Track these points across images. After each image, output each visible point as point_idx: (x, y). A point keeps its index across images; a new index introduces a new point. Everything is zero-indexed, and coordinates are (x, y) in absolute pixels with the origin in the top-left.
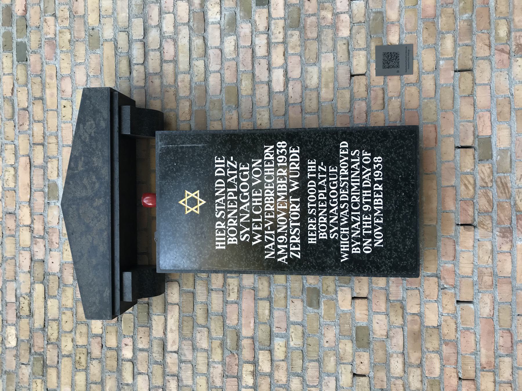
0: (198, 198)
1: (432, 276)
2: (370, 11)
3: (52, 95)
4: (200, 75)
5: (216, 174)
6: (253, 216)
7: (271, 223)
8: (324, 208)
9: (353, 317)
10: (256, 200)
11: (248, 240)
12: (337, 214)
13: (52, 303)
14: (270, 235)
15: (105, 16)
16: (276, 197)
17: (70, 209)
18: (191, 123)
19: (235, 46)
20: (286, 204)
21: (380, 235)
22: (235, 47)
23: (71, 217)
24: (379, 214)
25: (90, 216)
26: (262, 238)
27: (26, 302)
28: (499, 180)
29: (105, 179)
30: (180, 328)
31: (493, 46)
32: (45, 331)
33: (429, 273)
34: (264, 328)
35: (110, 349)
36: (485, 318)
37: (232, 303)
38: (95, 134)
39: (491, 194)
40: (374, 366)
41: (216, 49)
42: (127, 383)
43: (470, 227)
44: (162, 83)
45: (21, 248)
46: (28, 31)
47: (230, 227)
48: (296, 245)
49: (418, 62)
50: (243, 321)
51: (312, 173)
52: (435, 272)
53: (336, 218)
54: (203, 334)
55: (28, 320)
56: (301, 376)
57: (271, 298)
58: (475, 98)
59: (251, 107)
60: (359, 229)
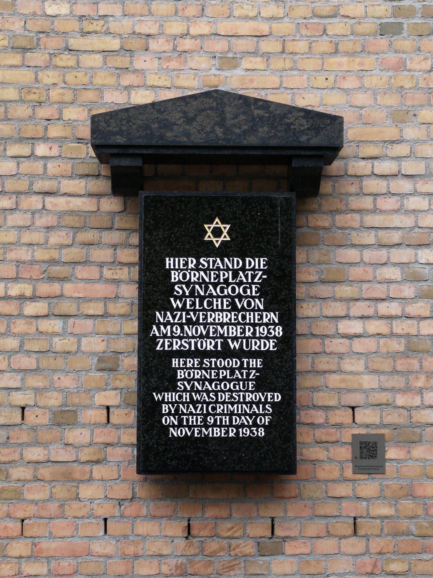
0: (222, 239)
1: (133, 493)
2: (423, 429)
3: (339, 64)
4: (358, 239)
5: (247, 259)
6: (202, 299)
7: (194, 319)
8: (211, 376)
9: (86, 407)
10: (219, 303)
11: (175, 293)
12: (204, 389)
13: (96, 60)
14: (181, 318)
15: (429, 130)
16: (222, 325)
17: (212, 100)
18: (304, 228)
19: (390, 279)
20: (215, 335)
21: (181, 433)
22: (388, 280)
23: (203, 101)
24: (204, 433)
25: (205, 122)
26: (178, 309)
27: (98, 29)
28: (237, 562)
29: (244, 139)
30: (71, 213)
31: (380, 556)
32: (65, 50)
33: (137, 489)
34: (73, 310)
35: (46, 129)
36: (89, 548)
37: (101, 272)
38: (293, 129)
39: (222, 555)
40: (34, 429)
41: (386, 258)
42: (7, 149)
43: (187, 533)
44: (351, 195)
45: (162, 23)
46: (415, 38)
47: (190, 273)
48: (171, 345)
49: (365, 480)
50: (81, 285)
51: (248, 363)
52: (137, 496)
53: (200, 389)
54: (65, 238)
55: (78, 30)
56: (20, 350)
57: (107, 317)
58: (326, 538)
59: (321, 297)
60: (188, 412)
